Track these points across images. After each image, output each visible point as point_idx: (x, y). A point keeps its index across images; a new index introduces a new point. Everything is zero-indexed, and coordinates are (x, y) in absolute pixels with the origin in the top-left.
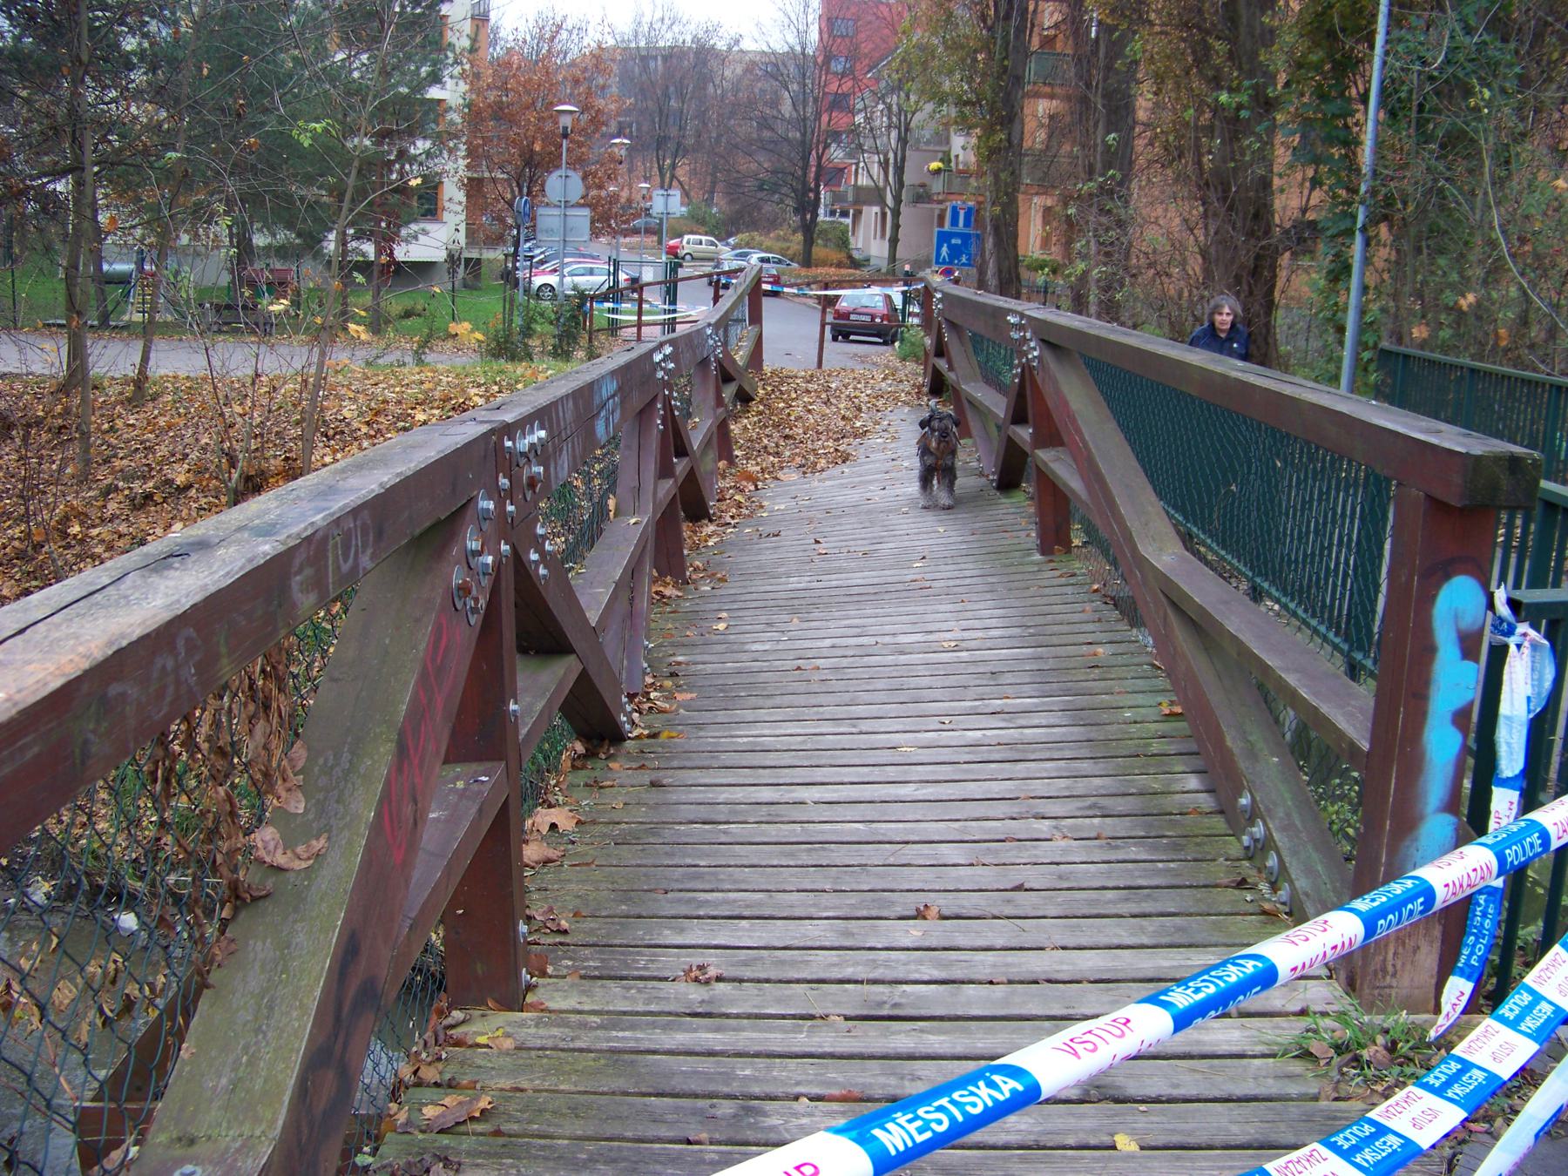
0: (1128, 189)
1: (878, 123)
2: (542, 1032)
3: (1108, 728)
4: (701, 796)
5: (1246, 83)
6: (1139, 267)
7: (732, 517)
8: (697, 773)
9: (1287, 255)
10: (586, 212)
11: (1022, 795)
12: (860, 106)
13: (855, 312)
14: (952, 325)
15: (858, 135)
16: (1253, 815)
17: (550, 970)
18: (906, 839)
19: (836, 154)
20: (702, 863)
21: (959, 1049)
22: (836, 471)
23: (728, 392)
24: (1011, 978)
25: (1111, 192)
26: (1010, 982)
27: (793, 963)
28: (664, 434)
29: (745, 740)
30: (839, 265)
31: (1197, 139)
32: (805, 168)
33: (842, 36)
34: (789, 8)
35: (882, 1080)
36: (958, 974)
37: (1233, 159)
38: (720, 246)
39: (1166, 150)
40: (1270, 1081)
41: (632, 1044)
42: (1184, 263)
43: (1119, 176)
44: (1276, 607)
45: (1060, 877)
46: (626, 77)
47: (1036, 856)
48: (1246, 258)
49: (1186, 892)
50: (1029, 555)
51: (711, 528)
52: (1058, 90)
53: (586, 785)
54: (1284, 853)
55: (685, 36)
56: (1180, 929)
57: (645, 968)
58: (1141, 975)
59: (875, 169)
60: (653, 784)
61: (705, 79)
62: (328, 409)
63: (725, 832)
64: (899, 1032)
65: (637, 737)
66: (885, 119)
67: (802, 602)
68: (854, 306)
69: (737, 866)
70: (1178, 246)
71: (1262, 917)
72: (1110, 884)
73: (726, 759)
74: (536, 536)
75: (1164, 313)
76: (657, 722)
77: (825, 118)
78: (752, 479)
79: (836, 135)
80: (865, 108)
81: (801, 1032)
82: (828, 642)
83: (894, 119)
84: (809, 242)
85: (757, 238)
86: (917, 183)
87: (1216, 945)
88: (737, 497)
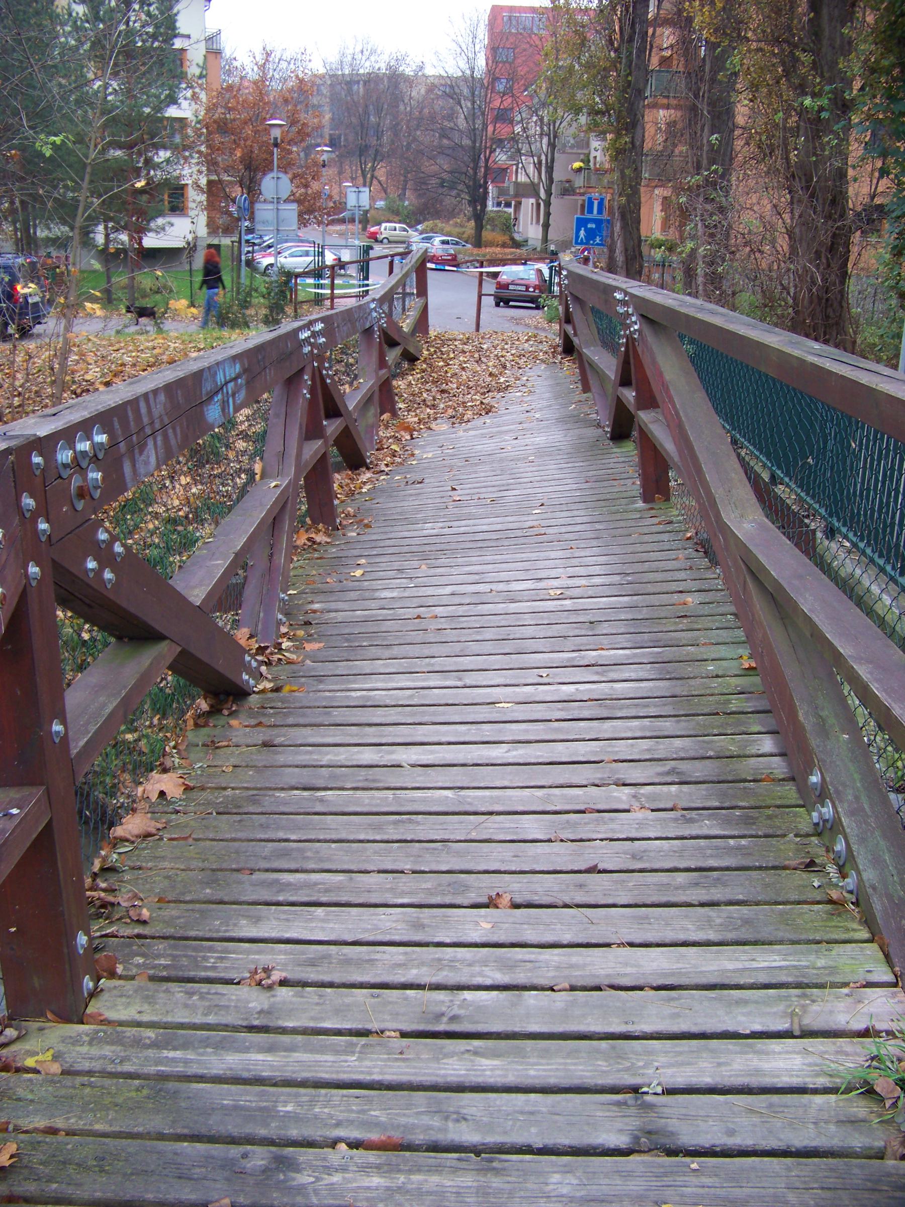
0: (729, 181)
1: (532, 132)
2: (95, 1051)
3: (692, 682)
4: (307, 757)
5: (827, 88)
6: (736, 246)
7: (387, 465)
8: (308, 731)
9: (858, 233)
10: (294, 206)
11: (606, 758)
12: (518, 118)
13: (513, 283)
14: (576, 299)
15: (517, 142)
16: (822, 795)
17: (120, 969)
18: (490, 809)
19: (501, 158)
20: (293, 837)
21: (511, 1079)
22: (478, 422)
23: (392, 356)
24: (575, 982)
25: (714, 184)
26: (573, 988)
27: (359, 963)
28: (312, 403)
29: (359, 694)
30: (504, 245)
31: (785, 139)
32: (476, 168)
33: (504, 63)
34: (460, 39)
35: (426, 1120)
36: (521, 978)
37: (815, 154)
38: (411, 232)
39: (759, 147)
40: (832, 1128)
41: (180, 1069)
42: (773, 242)
43: (720, 171)
44: (848, 544)
45: (634, 857)
46: (334, 99)
47: (613, 830)
48: (824, 237)
49: (754, 874)
50: (634, 503)
51: (368, 475)
52: (673, 102)
53: (203, 745)
54: (852, 840)
55: (380, 64)
56: (746, 922)
57: (214, 968)
58: (703, 981)
59: (531, 169)
60: (265, 744)
61: (396, 98)
62: (77, 371)
63: (321, 800)
64: (451, 1055)
65: (263, 691)
66: (538, 128)
67: (433, 548)
68: (512, 279)
69: (326, 841)
70: (769, 227)
71: (829, 907)
72: (682, 865)
73: (338, 715)
74: (97, 543)
75: (757, 283)
76: (283, 672)
77: (490, 128)
78: (410, 430)
79: (500, 142)
80: (522, 120)
81: (353, 1053)
82: (448, 590)
83: (545, 128)
84: (479, 228)
85: (440, 225)
86: (564, 179)
87: (781, 942)
88: (393, 447)
